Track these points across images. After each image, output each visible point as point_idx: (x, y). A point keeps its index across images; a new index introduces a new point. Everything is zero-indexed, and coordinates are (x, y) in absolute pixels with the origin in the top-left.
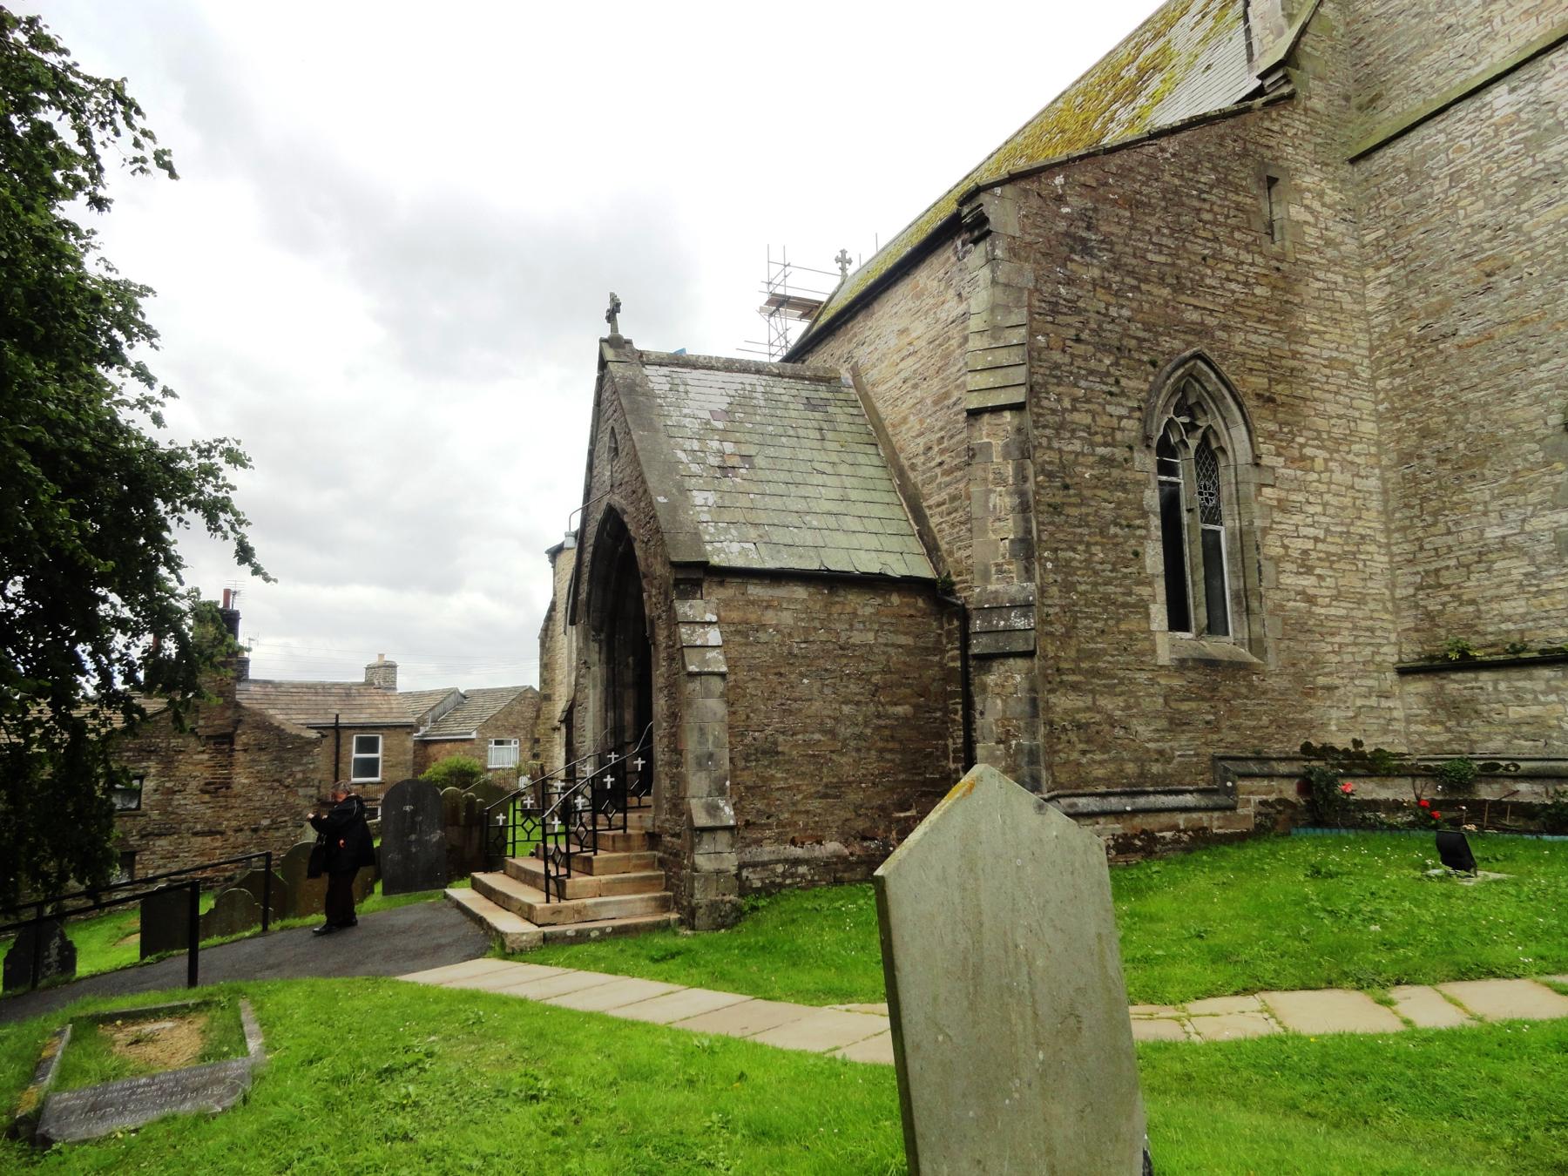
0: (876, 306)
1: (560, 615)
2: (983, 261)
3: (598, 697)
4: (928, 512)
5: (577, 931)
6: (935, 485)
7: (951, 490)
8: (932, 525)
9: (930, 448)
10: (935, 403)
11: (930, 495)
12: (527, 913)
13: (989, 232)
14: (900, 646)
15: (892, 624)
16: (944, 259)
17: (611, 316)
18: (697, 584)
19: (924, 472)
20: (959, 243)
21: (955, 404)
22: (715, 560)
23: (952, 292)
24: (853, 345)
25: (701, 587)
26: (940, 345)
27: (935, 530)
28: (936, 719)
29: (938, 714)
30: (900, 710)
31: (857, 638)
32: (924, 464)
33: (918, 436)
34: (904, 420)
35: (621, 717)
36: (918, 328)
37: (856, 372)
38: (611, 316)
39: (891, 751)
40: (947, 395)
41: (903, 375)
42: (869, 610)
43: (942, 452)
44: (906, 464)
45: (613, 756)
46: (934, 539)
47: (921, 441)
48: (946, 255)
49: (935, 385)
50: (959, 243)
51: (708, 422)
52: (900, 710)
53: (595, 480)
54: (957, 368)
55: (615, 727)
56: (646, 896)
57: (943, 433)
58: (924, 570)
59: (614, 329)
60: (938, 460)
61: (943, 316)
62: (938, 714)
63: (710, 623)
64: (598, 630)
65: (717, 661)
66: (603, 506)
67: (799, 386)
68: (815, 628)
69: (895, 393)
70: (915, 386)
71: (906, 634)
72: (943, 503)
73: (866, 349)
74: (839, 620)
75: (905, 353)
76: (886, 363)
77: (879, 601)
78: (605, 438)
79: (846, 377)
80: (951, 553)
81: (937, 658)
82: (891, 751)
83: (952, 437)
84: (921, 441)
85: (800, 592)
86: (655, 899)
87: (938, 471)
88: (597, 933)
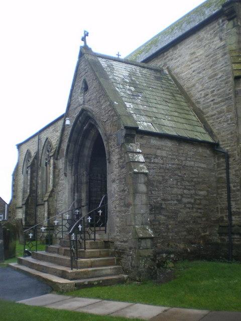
0: (178, 46)
1: (20, 168)
2: (232, 27)
3: (70, 188)
4: (206, 119)
5: (89, 282)
6: (210, 109)
7: (219, 110)
8: (209, 124)
9: (208, 95)
10: (210, 78)
11: (208, 112)
12: (63, 275)
13: (235, 17)
14: (202, 168)
15: (200, 159)
16: (215, 25)
17: (84, 39)
18: (133, 137)
19: (204, 104)
20: (221, 21)
21: (220, 78)
22: (140, 128)
23: (217, 38)
24: (166, 61)
25: (134, 137)
26: (212, 57)
27: (211, 125)
28: (214, 197)
29: (215, 195)
30: (202, 193)
31: (188, 163)
32: (204, 101)
33: (201, 91)
34: (194, 85)
35: (80, 196)
36: (200, 52)
37: (170, 71)
38: (84, 39)
39: (200, 209)
40: (216, 75)
41: (193, 69)
42: (192, 153)
43: (214, 96)
44: (194, 101)
45: (77, 211)
46: (211, 129)
47: (203, 93)
48: (215, 25)
49: (210, 72)
50: (221, 21)
51: (123, 79)
52: (202, 193)
53: (72, 101)
54: (221, 64)
55: (78, 200)
56: (112, 267)
57: (214, 89)
58: (209, 139)
59: (85, 43)
60: (212, 99)
61: (213, 47)
62: (215, 195)
63: (139, 153)
64: (71, 161)
65: (143, 168)
66: (79, 109)
67: (151, 72)
68: (174, 159)
69: (189, 76)
70: (199, 73)
71: (204, 163)
72: (215, 115)
73: (174, 61)
74: (182, 156)
75: (193, 61)
76: (184, 65)
77: (195, 150)
78: (80, 84)
79: (166, 71)
80: (219, 134)
81: (214, 174)
82: (200, 209)
83: (219, 90)
84: (203, 93)
85: (169, 144)
86: (115, 268)
87: (212, 103)
88: (96, 283)
